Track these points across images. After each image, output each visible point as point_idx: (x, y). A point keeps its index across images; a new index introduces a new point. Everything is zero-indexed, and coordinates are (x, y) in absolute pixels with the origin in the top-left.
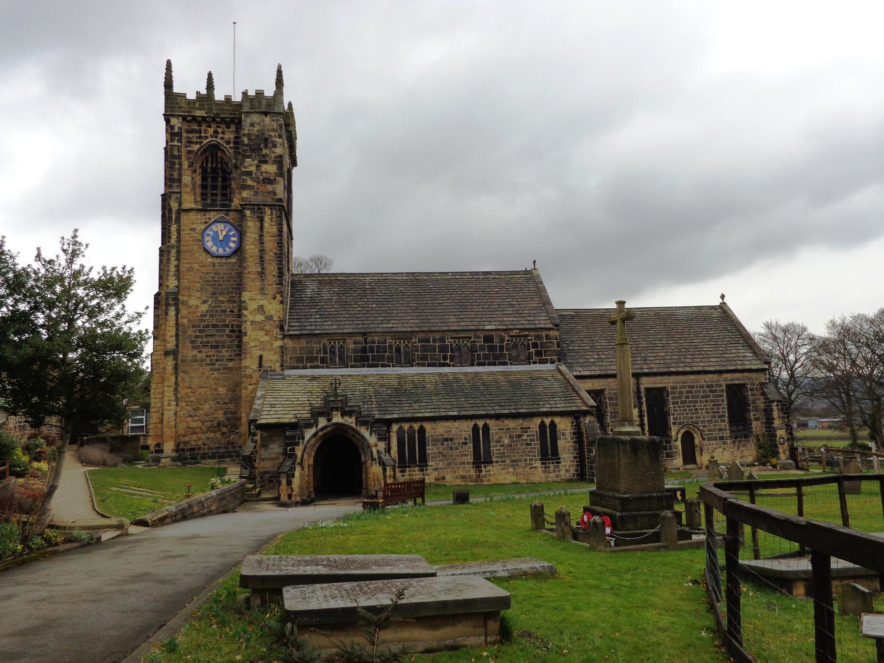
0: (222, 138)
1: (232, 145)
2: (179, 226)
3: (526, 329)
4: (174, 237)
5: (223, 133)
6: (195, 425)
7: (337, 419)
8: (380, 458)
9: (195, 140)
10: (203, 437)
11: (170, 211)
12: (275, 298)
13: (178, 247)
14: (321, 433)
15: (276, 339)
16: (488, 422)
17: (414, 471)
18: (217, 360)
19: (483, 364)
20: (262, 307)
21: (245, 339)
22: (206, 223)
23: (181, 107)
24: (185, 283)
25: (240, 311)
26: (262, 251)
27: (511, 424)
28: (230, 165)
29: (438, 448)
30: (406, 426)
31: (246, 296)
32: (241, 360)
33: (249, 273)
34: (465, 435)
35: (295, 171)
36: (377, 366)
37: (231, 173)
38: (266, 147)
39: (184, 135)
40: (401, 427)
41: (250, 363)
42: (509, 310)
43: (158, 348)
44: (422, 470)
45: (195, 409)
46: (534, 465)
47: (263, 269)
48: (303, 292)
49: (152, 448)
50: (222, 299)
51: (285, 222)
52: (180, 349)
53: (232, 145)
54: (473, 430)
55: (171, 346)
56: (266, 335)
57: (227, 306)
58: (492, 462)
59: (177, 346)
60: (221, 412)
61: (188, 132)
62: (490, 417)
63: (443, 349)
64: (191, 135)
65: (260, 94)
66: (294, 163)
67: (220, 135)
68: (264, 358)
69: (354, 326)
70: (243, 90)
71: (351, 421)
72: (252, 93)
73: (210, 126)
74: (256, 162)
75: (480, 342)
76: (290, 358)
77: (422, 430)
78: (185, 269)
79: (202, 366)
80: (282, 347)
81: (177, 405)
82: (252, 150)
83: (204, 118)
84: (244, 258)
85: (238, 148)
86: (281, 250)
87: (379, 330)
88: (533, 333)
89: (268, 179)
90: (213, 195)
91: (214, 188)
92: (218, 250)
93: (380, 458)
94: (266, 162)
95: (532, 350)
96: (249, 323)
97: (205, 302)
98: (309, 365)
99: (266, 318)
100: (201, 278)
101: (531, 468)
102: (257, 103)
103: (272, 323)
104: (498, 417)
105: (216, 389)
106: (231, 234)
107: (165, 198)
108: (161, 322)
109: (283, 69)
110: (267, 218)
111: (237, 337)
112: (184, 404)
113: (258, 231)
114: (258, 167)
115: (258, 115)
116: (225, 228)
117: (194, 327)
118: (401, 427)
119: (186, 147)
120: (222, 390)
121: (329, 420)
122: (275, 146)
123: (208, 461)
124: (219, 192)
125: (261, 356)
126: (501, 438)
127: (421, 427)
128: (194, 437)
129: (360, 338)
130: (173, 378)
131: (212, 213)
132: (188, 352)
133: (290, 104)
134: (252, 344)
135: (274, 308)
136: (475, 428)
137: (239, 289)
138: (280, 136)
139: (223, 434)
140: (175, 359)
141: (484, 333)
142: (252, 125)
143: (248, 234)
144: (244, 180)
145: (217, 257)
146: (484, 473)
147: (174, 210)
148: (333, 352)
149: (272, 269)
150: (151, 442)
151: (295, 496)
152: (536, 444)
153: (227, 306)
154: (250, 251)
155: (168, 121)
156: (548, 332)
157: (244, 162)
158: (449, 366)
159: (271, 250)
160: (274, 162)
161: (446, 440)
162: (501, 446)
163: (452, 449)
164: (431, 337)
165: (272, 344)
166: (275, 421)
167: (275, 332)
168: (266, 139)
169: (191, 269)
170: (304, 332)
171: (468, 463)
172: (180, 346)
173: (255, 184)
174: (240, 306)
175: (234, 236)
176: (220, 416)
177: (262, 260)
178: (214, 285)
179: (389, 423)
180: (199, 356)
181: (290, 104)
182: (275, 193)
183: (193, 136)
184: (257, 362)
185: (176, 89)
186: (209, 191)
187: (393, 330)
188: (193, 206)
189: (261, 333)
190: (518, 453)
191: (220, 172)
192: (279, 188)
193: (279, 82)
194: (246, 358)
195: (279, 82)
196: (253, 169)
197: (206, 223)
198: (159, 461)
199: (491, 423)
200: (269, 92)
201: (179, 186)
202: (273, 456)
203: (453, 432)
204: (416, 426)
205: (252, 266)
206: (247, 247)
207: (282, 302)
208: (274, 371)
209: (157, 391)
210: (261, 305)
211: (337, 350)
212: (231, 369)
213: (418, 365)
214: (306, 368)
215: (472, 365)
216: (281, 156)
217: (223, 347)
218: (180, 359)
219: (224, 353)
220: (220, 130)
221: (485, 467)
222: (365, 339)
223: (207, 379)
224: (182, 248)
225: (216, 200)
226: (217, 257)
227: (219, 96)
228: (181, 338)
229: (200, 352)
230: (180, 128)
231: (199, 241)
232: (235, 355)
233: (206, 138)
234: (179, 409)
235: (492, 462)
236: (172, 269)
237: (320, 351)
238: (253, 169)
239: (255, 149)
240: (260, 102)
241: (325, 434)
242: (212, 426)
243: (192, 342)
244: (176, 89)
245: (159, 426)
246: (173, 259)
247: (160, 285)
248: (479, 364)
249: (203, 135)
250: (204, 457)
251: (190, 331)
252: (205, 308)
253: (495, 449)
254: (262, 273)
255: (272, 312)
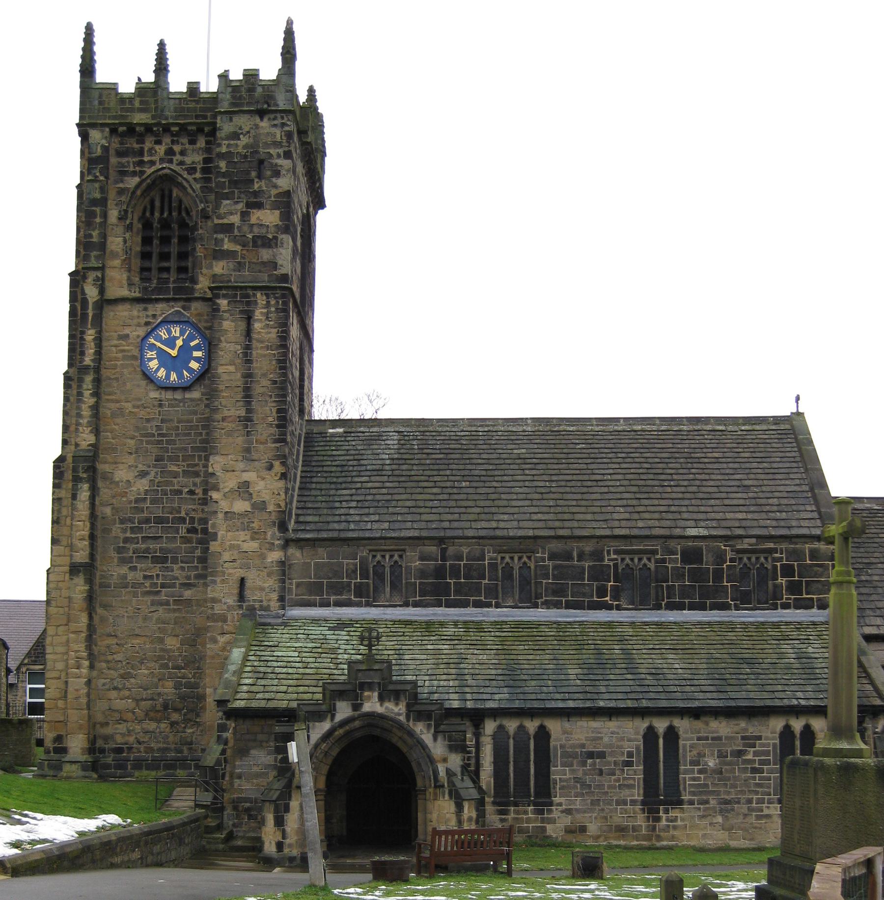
0: (181, 163)
1: (198, 175)
2: (100, 332)
3: (771, 538)
4: (90, 352)
5: (182, 153)
6: (119, 704)
7: (372, 704)
8: (451, 783)
9: (132, 169)
10: (138, 728)
11: (85, 302)
12: (270, 467)
13: (97, 370)
14: (341, 732)
15: (272, 547)
16: (677, 722)
17: (526, 813)
18: (163, 586)
19: (680, 607)
20: (246, 484)
21: (214, 546)
22: (147, 324)
23: (108, 109)
24: (107, 437)
25: (205, 492)
26: (248, 376)
27: (722, 727)
28: (194, 213)
29: (573, 771)
30: (512, 725)
31: (217, 463)
32: (206, 585)
33: (224, 419)
34: (629, 746)
35: (322, 218)
36: (465, 604)
37: (195, 228)
38: (260, 177)
39: (114, 160)
40: (501, 727)
41: (222, 592)
42: (739, 497)
43: (59, 561)
44: (541, 812)
45: (122, 676)
46: (766, 812)
47: (249, 411)
48: (331, 457)
49: (48, 743)
50: (175, 469)
51: (294, 320)
52: (98, 563)
53: (198, 175)
54: (645, 737)
55: (81, 556)
56: (253, 539)
57: (184, 483)
58: (680, 802)
59: (92, 556)
60: (170, 684)
61: (120, 154)
62: (682, 712)
63: (599, 574)
64: (124, 160)
65: (251, 76)
66: (320, 203)
67: (178, 157)
68: (249, 584)
69: (423, 525)
70: (221, 71)
71: (396, 709)
72: (236, 75)
73: (158, 142)
74: (240, 206)
75: (675, 562)
76: (298, 585)
77: (543, 735)
78: (109, 412)
79: (135, 595)
80: (282, 563)
81: (92, 667)
82: (234, 183)
83: (148, 128)
84: (216, 390)
85: (208, 180)
86: (285, 375)
87: (470, 533)
88: (784, 546)
89: (263, 238)
90: (161, 270)
91: (164, 257)
92: (168, 376)
93: (451, 783)
94: (259, 206)
95: (782, 581)
96: (221, 516)
97: (143, 474)
98: (333, 598)
99: (254, 506)
100: (137, 428)
101: (759, 817)
102: (250, 96)
103: (265, 516)
104: (696, 713)
105: (161, 640)
106: (192, 344)
107: (77, 279)
108: (64, 511)
109: (295, 28)
110: (258, 314)
111: (200, 542)
112: (104, 665)
113: (242, 339)
114: (244, 215)
115: (247, 116)
116: (182, 333)
117: (122, 522)
118: (501, 727)
119: (116, 182)
120: (172, 643)
121: (356, 707)
122: (277, 174)
123: (145, 772)
124: (173, 264)
125: (242, 581)
126: (701, 755)
127: (542, 728)
128: (122, 728)
129: (433, 549)
130: (84, 619)
131: (160, 306)
132: (114, 570)
133: (311, 91)
134: (226, 556)
135: (268, 487)
136: (650, 735)
137: (205, 449)
138: (288, 155)
139: (173, 724)
140: (90, 581)
141: (683, 542)
142: (235, 136)
143: (223, 345)
144: (218, 242)
145: (166, 389)
146: (664, 822)
147: (91, 302)
148: (379, 576)
149: (266, 411)
150: (49, 737)
151: (290, 846)
152: (771, 771)
153: (184, 483)
154: (225, 377)
155: (84, 136)
156: (816, 545)
157: (217, 206)
158: (609, 607)
159: (264, 375)
160: (275, 206)
161: (591, 755)
162: (700, 772)
163: (601, 773)
164: (575, 548)
165: (263, 557)
166: (263, 704)
167: (269, 534)
168: (261, 162)
169: (121, 412)
170: (324, 535)
171: (633, 802)
172: (98, 557)
173: (238, 248)
174: (206, 483)
175: (197, 348)
176: (168, 689)
177: (247, 395)
178: (159, 442)
179: (477, 717)
180: (131, 576)
181: (311, 91)
182: (275, 265)
183: (130, 162)
184: (236, 591)
185: (102, 76)
186: (154, 263)
187: (499, 533)
188: (125, 292)
189: (243, 535)
190: (734, 786)
191: (175, 226)
192: (285, 256)
193: (289, 54)
194: (214, 582)
195: (289, 54)
196: (235, 219)
197: (147, 324)
198: (60, 768)
199: (682, 725)
200: (269, 71)
201: (102, 256)
202: (255, 769)
203: (606, 739)
204: (531, 726)
205: (230, 407)
206: (221, 370)
207: (284, 476)
208: (267, 609)
209: (57, 640)
210: (246, 482)
211: (387, 570)
212: (188, 602)
213: (548, 605)
214: (328, 605)
215: (658, 607)
216: (288, 194)
217: (175, 560)
218: (97, 581)
219: (177, 573)
220: (177, 148)
221: (666, 811)
222: (444, 551)
223: (145, 619)
224: (105, 373)
225: (167, 281)
226: (166, 389)
227: (177, 84)
228: (99, 542)
229: (133, 569)
230: (105, 149)
231: (134, 358)
232: (198, 577)
233: (152, 163)
234: (95, 673)
235: (680, 802)
236: (86, 412)
237: (355, 571)
238: (235, 219)
239: (240, 182)
240: (251, 90)
241: (347, 733)
242: (153, 709)
243: (119, 550)
244: (102, 76)
245: (61, 703)
246: (87, 393)
247: (65, 442)
248: (671, 607)
249: (146, 159)
250: (138, 764)
251: (116, 530)
252: (142, 485)
253: (688, 776)
254: (247, 420)
255: (266, 496)
